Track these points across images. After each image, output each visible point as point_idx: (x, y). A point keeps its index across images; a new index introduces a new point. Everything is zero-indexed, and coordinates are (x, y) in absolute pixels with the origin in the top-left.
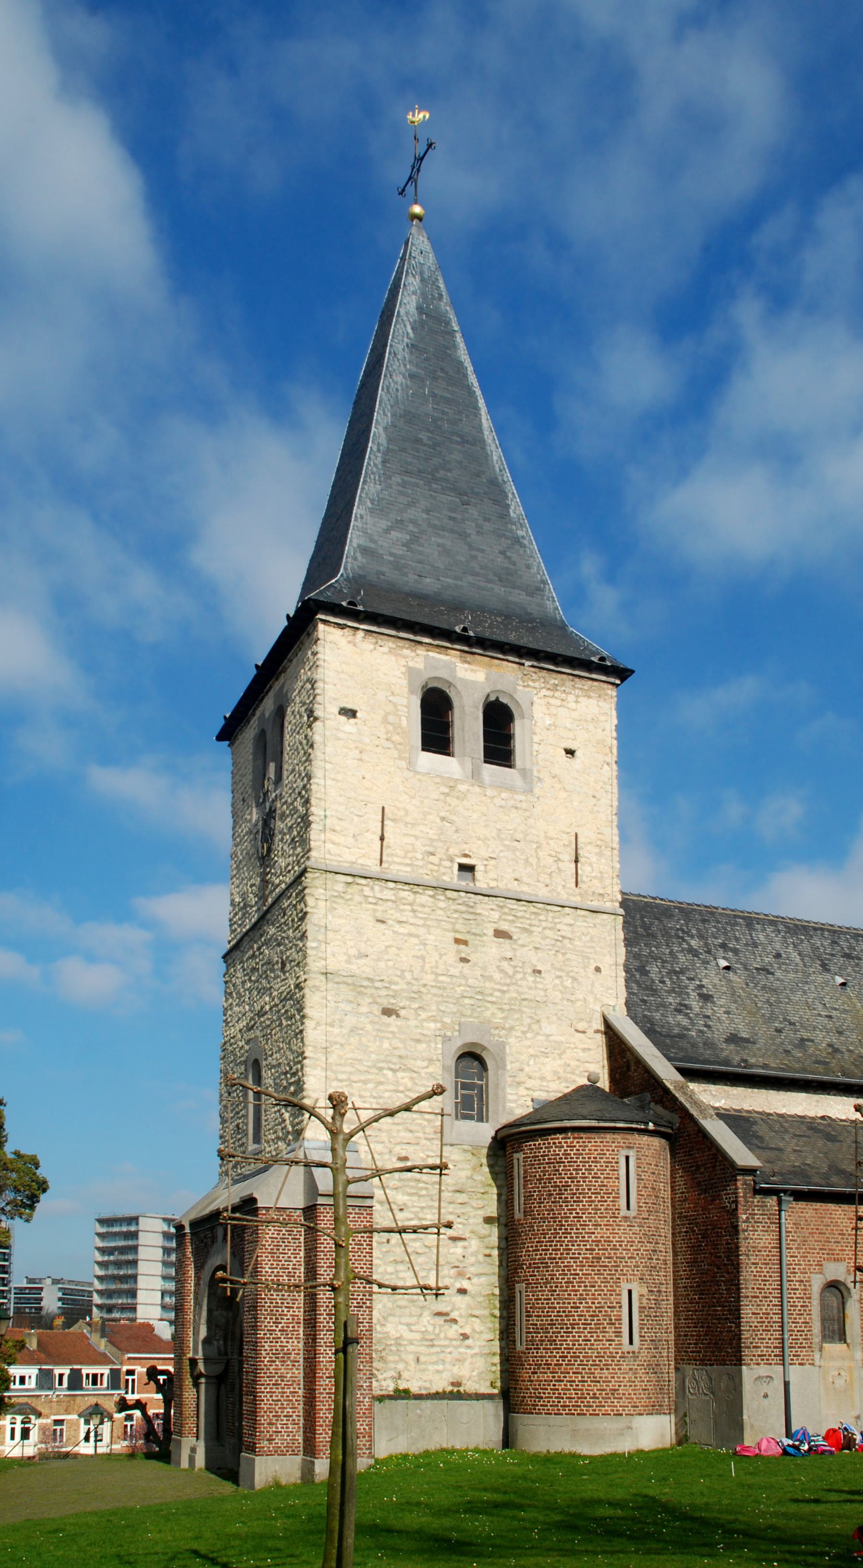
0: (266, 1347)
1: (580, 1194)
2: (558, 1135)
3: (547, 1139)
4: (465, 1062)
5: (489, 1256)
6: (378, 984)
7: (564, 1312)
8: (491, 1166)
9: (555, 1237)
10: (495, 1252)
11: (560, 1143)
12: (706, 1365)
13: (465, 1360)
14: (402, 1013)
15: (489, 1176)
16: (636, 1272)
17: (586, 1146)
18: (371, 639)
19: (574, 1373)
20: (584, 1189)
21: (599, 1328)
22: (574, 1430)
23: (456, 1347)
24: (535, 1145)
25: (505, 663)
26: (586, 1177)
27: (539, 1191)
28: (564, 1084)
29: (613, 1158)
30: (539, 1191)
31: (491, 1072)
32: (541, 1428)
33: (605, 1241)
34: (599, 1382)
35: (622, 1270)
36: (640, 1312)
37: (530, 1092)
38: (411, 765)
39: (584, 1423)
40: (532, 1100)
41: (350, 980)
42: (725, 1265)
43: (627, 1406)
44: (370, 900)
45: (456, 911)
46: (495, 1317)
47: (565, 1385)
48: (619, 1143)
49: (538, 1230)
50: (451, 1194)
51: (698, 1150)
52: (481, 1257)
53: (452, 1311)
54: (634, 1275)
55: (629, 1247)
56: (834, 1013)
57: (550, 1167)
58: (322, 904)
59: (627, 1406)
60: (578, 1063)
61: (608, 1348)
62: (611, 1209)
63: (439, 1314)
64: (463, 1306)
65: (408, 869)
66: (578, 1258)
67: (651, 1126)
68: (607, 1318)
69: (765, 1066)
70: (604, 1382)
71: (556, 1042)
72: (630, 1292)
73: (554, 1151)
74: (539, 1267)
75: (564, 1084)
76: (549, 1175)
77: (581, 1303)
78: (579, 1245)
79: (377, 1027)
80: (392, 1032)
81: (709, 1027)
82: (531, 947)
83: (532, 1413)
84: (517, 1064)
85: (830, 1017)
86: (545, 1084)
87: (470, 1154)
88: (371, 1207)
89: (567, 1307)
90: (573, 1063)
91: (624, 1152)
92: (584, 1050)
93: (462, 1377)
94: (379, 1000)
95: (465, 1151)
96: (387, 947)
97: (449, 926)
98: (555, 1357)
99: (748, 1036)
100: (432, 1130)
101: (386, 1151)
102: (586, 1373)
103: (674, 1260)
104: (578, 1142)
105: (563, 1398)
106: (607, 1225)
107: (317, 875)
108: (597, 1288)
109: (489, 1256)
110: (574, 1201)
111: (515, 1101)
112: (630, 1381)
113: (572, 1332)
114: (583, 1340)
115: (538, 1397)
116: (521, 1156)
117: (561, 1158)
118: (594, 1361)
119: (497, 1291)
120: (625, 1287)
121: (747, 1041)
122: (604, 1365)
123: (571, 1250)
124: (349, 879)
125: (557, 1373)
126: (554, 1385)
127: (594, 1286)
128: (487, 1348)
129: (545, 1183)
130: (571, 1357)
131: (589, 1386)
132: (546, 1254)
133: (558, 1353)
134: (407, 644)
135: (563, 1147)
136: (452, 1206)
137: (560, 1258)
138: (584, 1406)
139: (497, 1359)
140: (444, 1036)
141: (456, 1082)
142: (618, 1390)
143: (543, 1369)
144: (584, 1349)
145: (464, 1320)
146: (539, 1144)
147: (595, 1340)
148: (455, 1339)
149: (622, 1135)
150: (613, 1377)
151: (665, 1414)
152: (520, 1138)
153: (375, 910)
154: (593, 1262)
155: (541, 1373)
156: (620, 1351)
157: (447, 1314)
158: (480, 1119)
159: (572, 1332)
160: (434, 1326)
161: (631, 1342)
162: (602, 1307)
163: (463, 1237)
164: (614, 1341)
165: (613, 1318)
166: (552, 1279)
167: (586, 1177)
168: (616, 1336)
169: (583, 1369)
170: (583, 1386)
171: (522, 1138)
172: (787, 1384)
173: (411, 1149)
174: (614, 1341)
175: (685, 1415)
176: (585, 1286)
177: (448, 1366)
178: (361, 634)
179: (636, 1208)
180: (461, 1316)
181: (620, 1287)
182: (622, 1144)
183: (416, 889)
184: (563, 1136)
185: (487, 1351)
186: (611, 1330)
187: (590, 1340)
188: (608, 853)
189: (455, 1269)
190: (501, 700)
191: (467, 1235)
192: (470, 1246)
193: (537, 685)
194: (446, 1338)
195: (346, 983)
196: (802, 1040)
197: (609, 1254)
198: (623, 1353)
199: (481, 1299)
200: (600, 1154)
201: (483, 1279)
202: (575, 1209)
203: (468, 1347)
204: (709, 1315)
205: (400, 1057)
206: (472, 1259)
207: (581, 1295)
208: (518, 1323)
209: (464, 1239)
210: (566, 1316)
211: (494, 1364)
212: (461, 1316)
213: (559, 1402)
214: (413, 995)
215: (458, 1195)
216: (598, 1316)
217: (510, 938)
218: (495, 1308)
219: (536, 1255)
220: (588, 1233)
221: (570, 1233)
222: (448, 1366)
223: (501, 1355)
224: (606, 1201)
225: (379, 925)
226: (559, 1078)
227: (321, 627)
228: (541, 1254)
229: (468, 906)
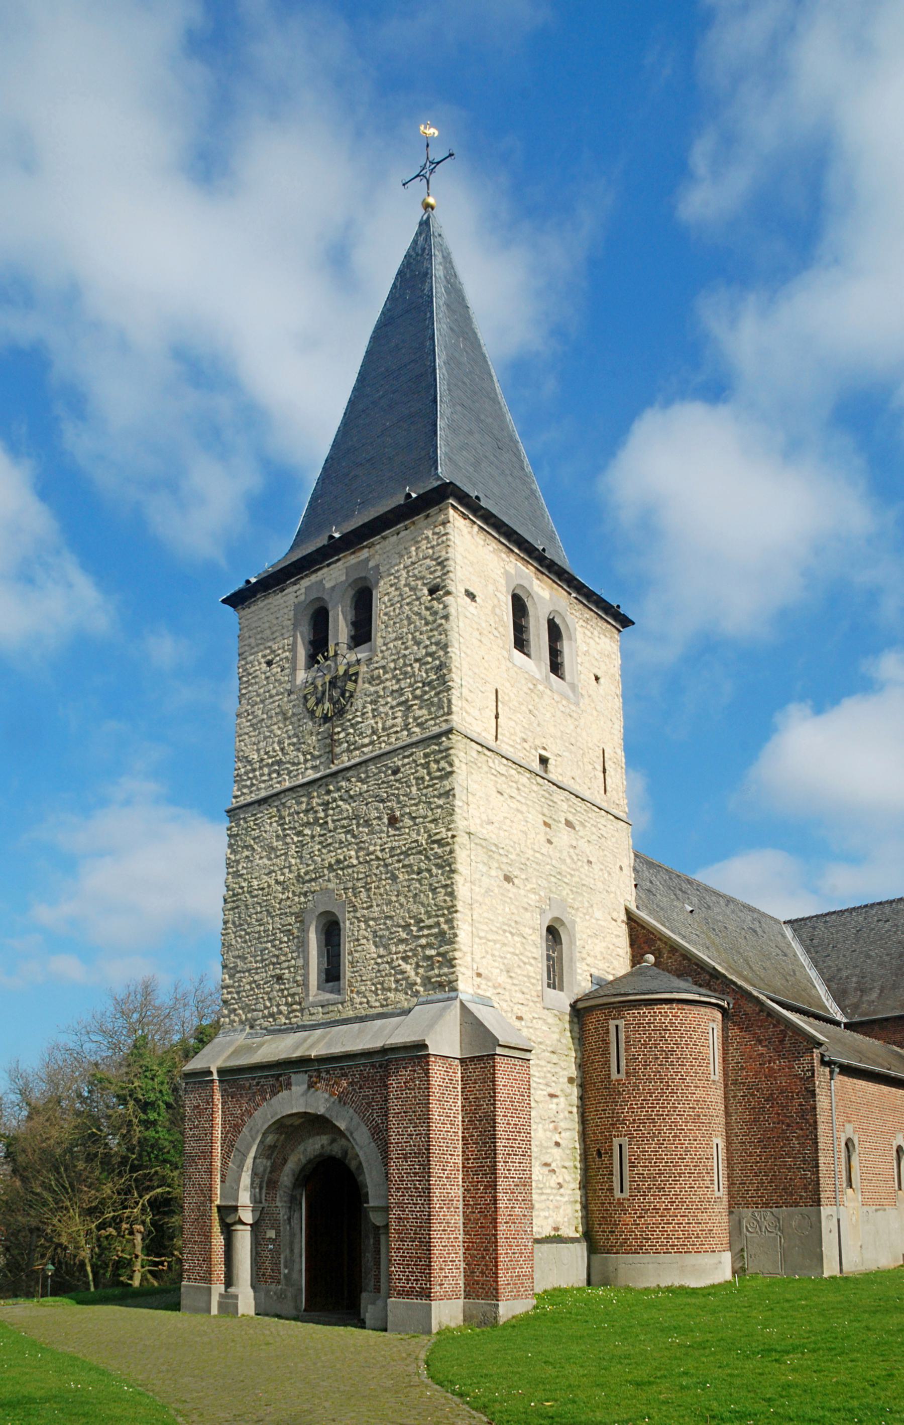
0: (437, 1194)
2: (664, 1006)
6: (501, 851)
10: (575, 1110)
11: (666, 1012)
12: (771, 1207)
14: (516, 881)
15: (570, 1040)
18: (482, 535)
22: (682, 1266)
25: (560, 589)
28: (607, 965)
31: (565, 946)
32: (650, 1266)
38: (510, 659)
39: (691, 1259)
40: (591, 976)
41: (484, 843)
42: (798, 1123)
44: (493, 771)
45: (543, 796)
52: (566, 1113)
58: (464, 767)
64: (559, 1158)
65: (511, 750)
79: (501, 891)
80: (510, 898)
82: (585, 840)
88: (529, 1060)
94: (503, 866)
96: (505, 818)
97: (539, 809)
100: (534, 994)
101: (509, 1009)
107: (460, 738)
111: (581, 975)
116: (622, 1023)
119: (577, 1146)
124: (479, 748)
134: (504, 549)
140: (541, 908)
153: (496, 782)
171: (624, 1007)
172: (839, 1220)
173: (524, 1008)
175: (742, 1250)
178: (476, 528)
180: (557, 1167)
183: (520, 769)
185: (572, 1199)
188: (619, 770)
190: (556, 620)
191: (558, 1093)
193: (577, 614)
195: (481, 846)
199: (568, 1152)
203: (562, 1195)
205: (516, 922)
206: (561, 1116)
211: (577, 1211)
214: (522, 866)
215: (552, 1055)
217: (574, 829)
219: (642, 1112)
223: (581, 1203)
225: (499, 796)
227: (451, 511)
229: (549, 793)
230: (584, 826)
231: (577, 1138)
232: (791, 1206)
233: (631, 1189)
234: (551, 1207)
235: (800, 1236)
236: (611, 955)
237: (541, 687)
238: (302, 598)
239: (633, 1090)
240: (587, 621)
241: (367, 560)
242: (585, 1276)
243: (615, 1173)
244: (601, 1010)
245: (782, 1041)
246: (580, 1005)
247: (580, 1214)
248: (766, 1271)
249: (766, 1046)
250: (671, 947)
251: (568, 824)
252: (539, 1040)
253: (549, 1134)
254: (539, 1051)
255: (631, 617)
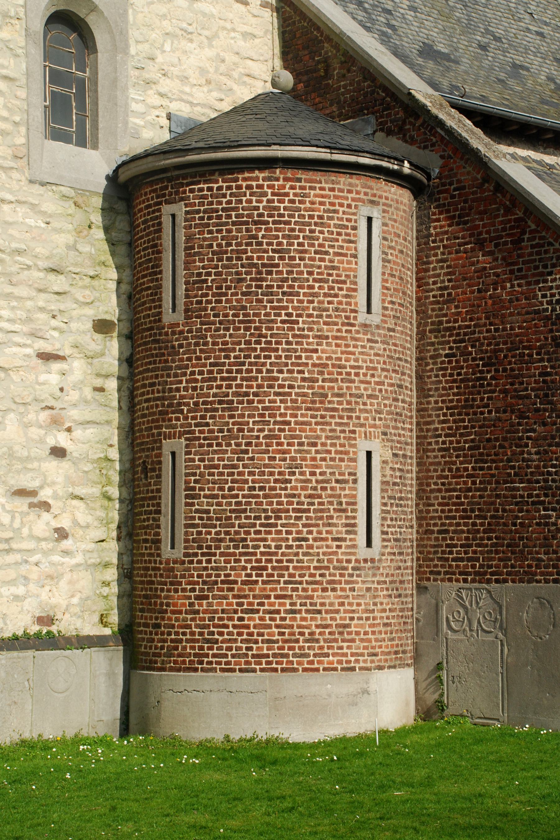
1: (294, 280)
3: (236, 180)
4: (59, 30)
5: (101, 390)
7: (262, 488)
8: (107, 229)
9: (247, 357)
10: (112, 385)
11: (260, 187)
12: (489, 581)
13: (60, 576)
15: (106, 247)
16: (377, 422)
17: (305, 195)
19: (277, 597)
20: (302, 273)
21: (321, 518)
23: (46, 553)
24: (210, 189)
26: (305, 251)
27: (218, 274)
28: (215, 94)
29: (349, 220)
30: (218, 274)
31: (102, 56)
32: (214, 696)
33: (334, 366)
34: (319, 612)
35: (358, 418)
36: (382, 490)
37: (165, 102)
40: (169, 117)
42: (537, 410)
43: (362, 655)
46: (110, 499)
47: (261, 619)
48: (358, 193)
49: (214, 344)
50: (42, 275)
51: (480, 213)
52: (88, 392)
53: (42, 487)
54: (374, 426)
55: (368, 378)
56: (546, 30)
57: (238, 231)
59: (362, 655)
60: (236, 59)
61: (336, 553)
62: (344, 310)
63: (21, 493)
64: (60, 479)
66: (290, 394)
67: (406, 168)
68: (335, 501)
69: (483, 98)
70: (327, 612)
71: (204, 14)
72: (369, 454)
73: (249, 201)
74: (216, 410)
75: (215, 94)
76: (237, 245)
77: (294, 474)
78: (289, 371)
81: (392, 27)
83: (196, 670)
84: (146, 46)
85: (541, 35)
86: (187, 89)
87: (71, 203)
89: (268, 481)
90: (230, 58)
91: (365, 211)
92: (246, 35)
93: (53, 607)
95: (65, 197)
98: (245, 568)
99: (446, 51)
102: (299, 597)
103: (419, 403)
104: (292, 188)
105: (256, 642)
106: (337, 338)
108: (319, 447)
109: (101, 390)
110: (284, 293)
111: (142, 115)
112: (367, 611)
113: (276, 525)
114: (294, 540)
115: (208, 641)
116: (180, 209)
117: (261, 215)
118: (312, 575)
119: (114, 454)
120: (363, 446)
121: (446, 57)
122: (329, 582)
123: (277, 379)
125: (246, 597)
126: (241, 619)
127: (314, 445)
128: (95, 555)
129: (229, 259)
130: (274, 568)
131: (303, 619)
132: (229, 387)
133: (249, 561)
135: (265, 194)
136: (43, 296)
137: (256, 394)
138: (294, 655)
139: (112, 574)
141: (45, 66)
142: (348, 626)
143: (220, 590)
144: (297, 554)
145: (60, 504)
146: (220, 188)
147: (315, 540)
148: (45, 539)
149: (363, 180)
150: (342, 604)
151: (408, 665)
152: (178, 178)
154: (313, 402)
155: (214, 597)
156: (353, 558)
157: (33, 493)
158: (81, 143)
159: (276, 525)
160: (12, 513)
161: (369, 544)
162: (327, 482)
163: (61, 353)
164: (344, 540)
165: (344, 500)
166: (240, 430)
167: (305, 251)
168: (348, 532)
169: (293, 590)
170: (294, 619)
171: (184, 177)
174: (344, 540)
175: (439, 667)
176: (301, 444)
177: (32, 587)
179: (381, 311)
180: (56, 496)
181: (354, 446)
182: (362, 196)
184: (266, 174)
185: (95, 560)
186: (340, 521)
187: (306, 540)
189: (48, 412)
191: (67, 351)
192: (71, 370)
194: (32, 537)
196: (515, 66)
197: (340, 388)
198: (357, 561)
199: (88, 467)
200: (328, 211)
201: (91, 432)
202: (286, 308)
203: (66, 553)
204: (498, 496)
206: (74, 396)
207: (293, 459)
208: (166, 507)
209: (62, 358)
210: (266, 496)
211: (106, 584)
212: (56, 496)
213: (249, 649)
215: (52, 277)
216: (320, 497)
218: (109, 483)
219: (210, 388)
220: (306, 351)
221: (277, 350)
222: (32, 587)
223: (120, 566)
224: (336, 296)
226: (208, 82)
228: (219, 387)
231: (115, 440)
232: (521, 581)
233: (186, 541)
234: (34, 576)
235: (535, 643)
236: (229, 76)
239: (197, 344)
242: (118, 714)
243: (163, 509)
244: (151, 183)
245: (517, 242)
246: (123, 177)
247: (115, 589)
248: (478, 713)
249: (491, 253)
250: (345, 54)
252: (14, 245)
253: (35, 433)
254: (15, 268)
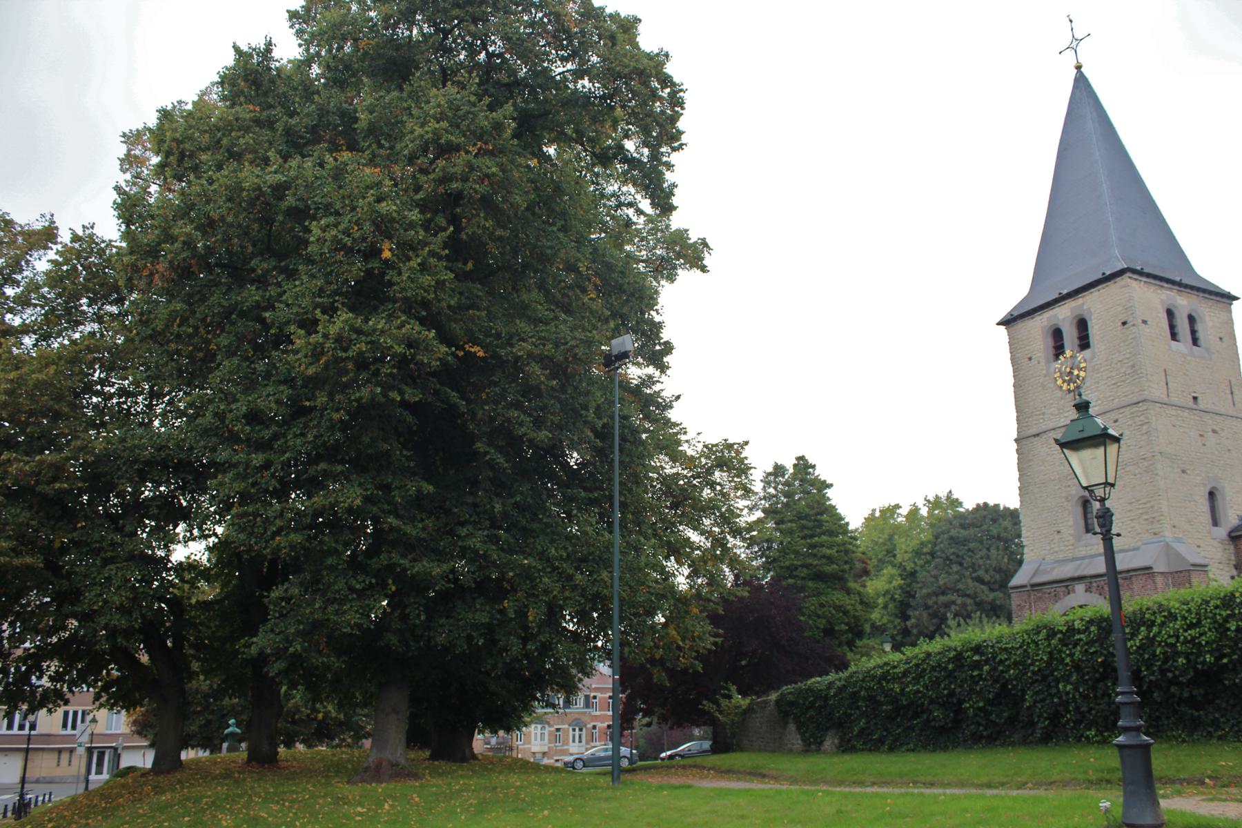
230: (1223, 430)
237: (1189, 358)
238: (1046, 323)
240: (1210, 307)
241: (1083, 304)
246: (1233, 534)
251: (1214, 431)
255: (1234, 293)
